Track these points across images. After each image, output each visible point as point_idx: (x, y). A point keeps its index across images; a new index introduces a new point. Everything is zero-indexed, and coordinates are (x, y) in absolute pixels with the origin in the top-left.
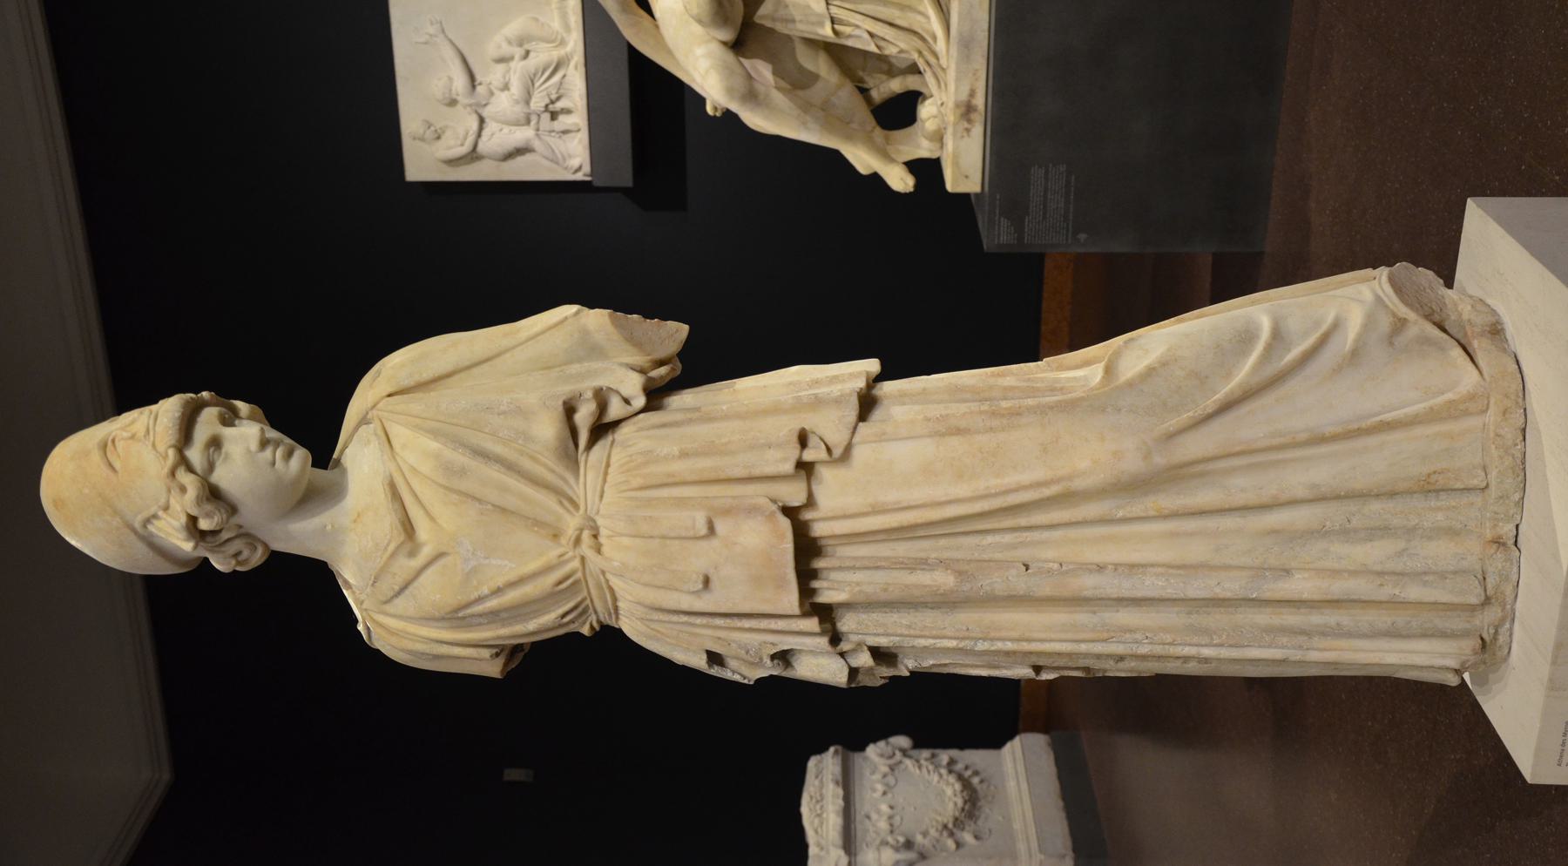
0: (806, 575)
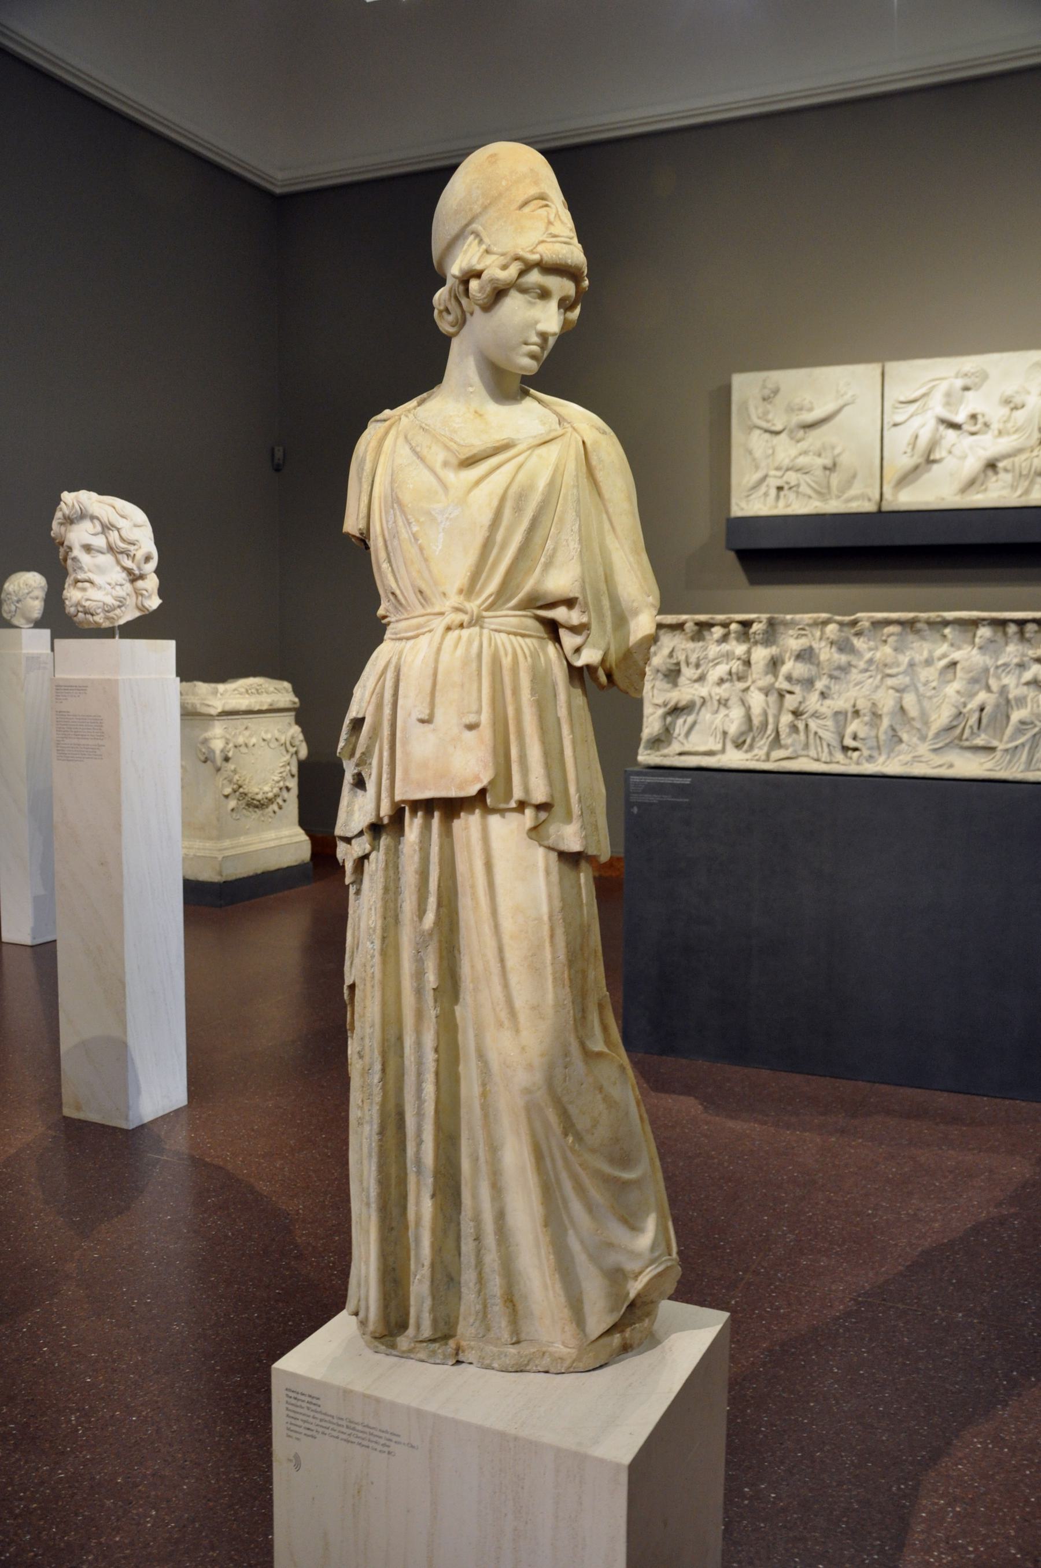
0: (428, 806)
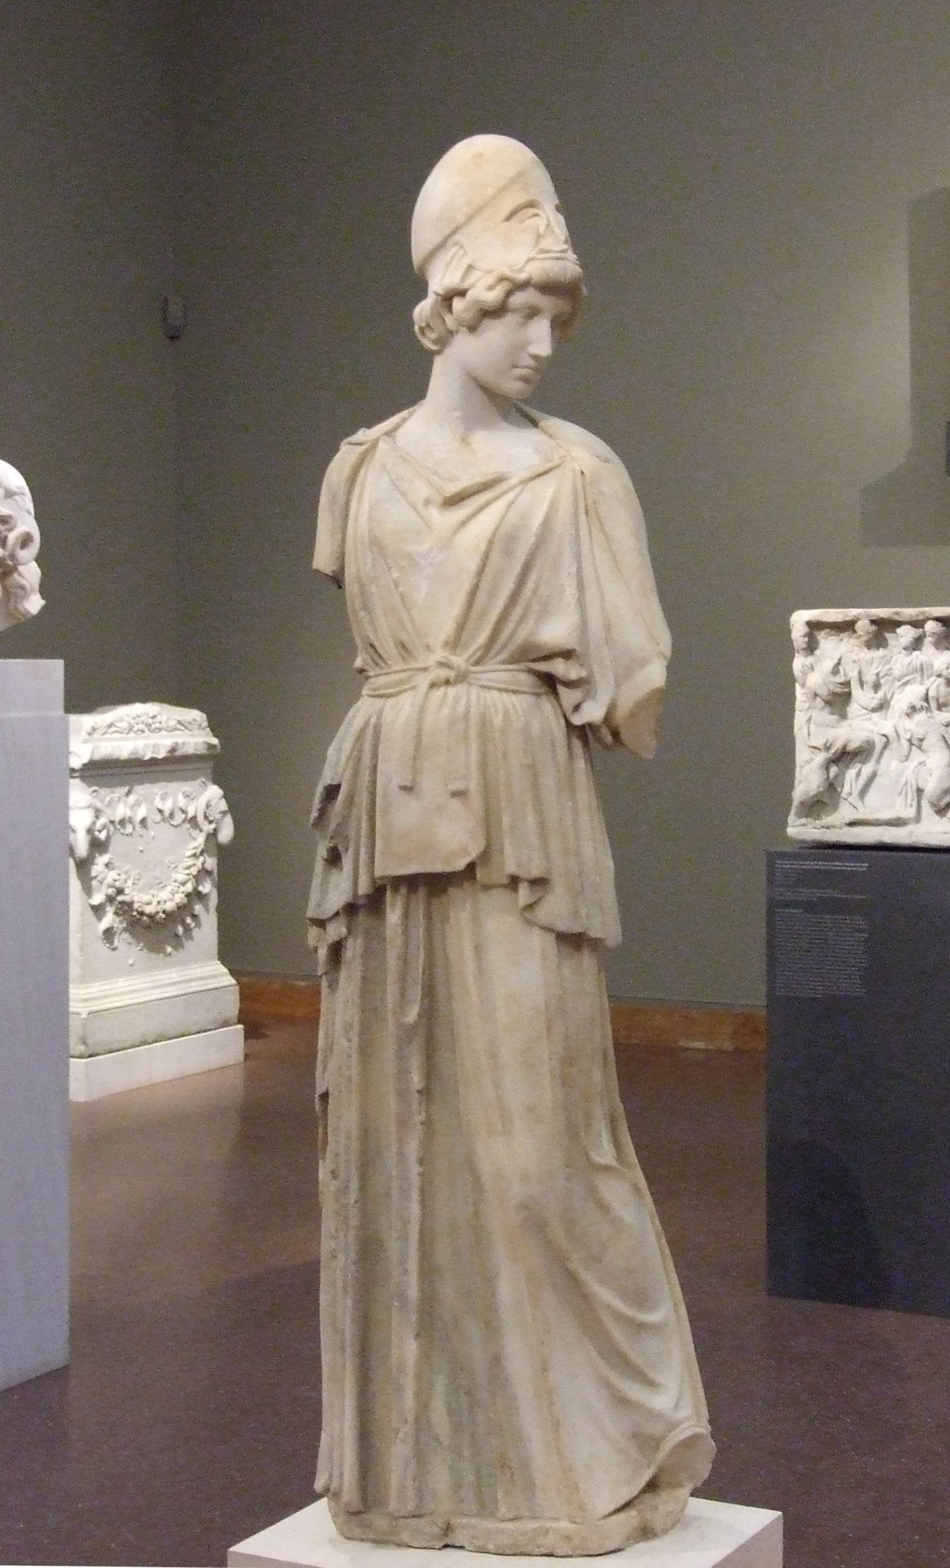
0: (411, 882)
